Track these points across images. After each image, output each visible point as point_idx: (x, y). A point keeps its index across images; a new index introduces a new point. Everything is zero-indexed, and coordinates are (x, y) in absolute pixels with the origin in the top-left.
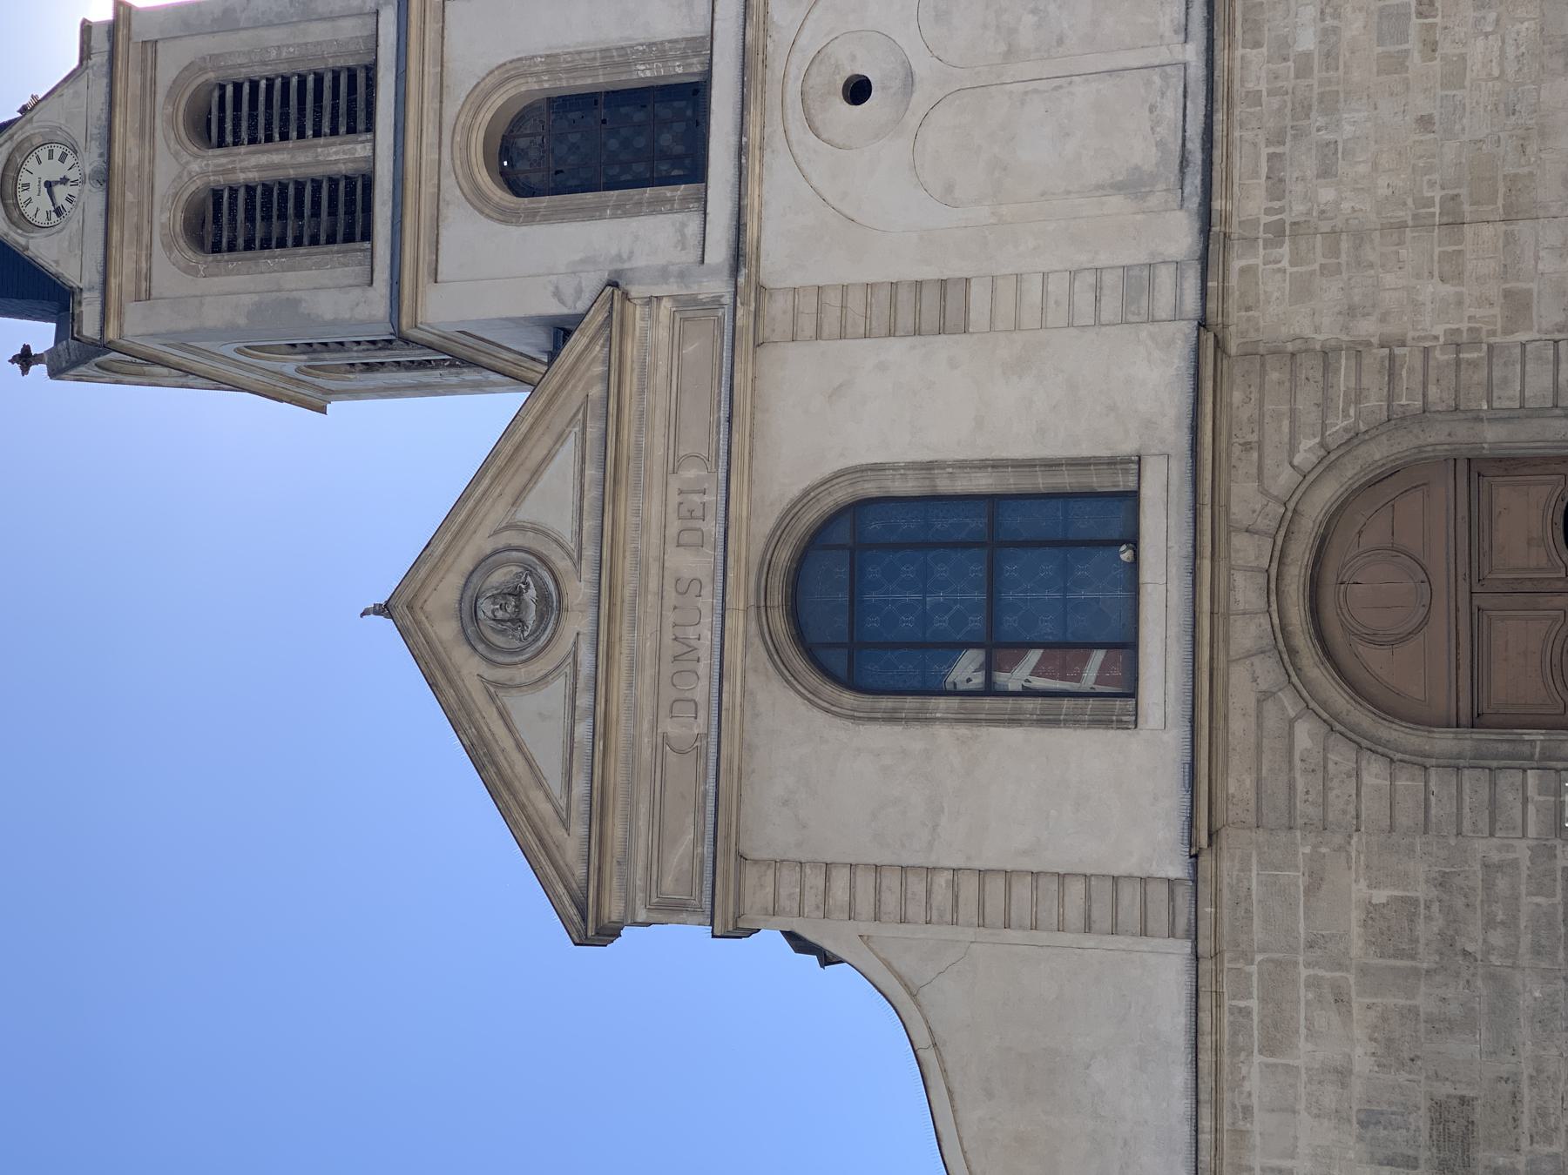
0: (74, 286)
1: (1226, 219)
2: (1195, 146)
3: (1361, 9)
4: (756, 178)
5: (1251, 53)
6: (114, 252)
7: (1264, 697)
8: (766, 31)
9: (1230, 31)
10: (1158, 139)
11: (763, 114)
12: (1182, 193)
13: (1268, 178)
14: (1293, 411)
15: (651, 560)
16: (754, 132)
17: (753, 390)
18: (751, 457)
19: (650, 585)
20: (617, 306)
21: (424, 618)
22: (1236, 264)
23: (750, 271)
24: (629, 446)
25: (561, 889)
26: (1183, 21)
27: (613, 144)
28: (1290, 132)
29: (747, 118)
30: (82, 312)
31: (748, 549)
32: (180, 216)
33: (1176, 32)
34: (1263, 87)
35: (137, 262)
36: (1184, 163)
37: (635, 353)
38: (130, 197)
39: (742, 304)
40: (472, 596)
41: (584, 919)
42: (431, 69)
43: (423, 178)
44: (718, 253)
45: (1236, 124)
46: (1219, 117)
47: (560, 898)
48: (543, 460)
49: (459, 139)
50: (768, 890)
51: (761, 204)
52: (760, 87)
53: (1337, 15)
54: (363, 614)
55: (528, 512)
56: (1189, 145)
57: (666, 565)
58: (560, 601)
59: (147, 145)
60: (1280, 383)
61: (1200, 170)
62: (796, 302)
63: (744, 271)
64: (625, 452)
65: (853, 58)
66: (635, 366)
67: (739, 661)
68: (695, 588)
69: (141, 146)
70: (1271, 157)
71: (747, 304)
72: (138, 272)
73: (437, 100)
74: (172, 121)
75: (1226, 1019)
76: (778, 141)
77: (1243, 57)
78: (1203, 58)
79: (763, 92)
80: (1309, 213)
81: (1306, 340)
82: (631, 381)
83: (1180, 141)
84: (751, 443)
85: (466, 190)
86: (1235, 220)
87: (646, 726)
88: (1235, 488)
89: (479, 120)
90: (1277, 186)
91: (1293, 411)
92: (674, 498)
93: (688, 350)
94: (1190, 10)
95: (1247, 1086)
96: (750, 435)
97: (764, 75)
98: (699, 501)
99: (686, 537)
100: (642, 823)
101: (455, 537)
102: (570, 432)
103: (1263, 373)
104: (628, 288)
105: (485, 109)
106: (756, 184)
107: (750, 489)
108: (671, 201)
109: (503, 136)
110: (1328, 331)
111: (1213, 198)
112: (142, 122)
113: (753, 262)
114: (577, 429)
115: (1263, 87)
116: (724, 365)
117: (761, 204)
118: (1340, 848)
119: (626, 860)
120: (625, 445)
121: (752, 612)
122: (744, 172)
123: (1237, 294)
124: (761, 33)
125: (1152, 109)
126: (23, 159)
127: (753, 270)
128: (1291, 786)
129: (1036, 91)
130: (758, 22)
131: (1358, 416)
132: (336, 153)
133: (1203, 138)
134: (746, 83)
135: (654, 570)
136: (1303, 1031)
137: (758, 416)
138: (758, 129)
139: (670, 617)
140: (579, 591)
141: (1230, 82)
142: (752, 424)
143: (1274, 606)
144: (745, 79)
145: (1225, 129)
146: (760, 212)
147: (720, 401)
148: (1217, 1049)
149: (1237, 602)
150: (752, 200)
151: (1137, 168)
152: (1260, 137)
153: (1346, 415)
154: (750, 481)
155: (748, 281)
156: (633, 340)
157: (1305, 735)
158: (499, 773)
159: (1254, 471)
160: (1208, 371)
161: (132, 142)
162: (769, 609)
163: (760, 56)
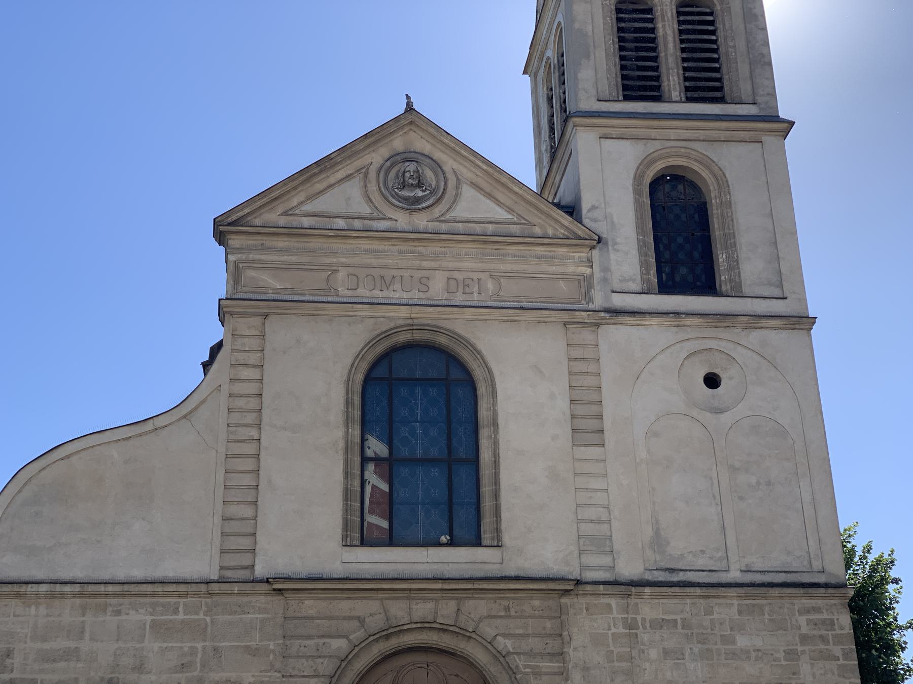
1: (639, 595)
2: (681, 577)
3: (761, 672)
5: (735, 609)
7: (361, 621)
8: (746, 328)
9: (747, 597)
10: (685, 556)
11: (698, 326)
12: (654, 570)
13: (663, 620)
14: (528, 635)
15: (440, 262)
16: (688, 321)
17: (539, 322)
18: (500, 321)
19: (425, 262)
20: (587, 242)
22: (613, 602)
25: (246, 211)
26: (753, 569)
27: (680, 240)
28: (689, 632)
29: (696, 317)
31: (446, 319)
33: (747, 565)
34: (715, 616)
36: (672, 570)
37: (560, 253)
39: (589, 315)
40: (418, 159)
41: (229, 224)
44: (619, 301)
45: (694, 601)
46: (698, 591)
47: (242, 210)
50: (247, 331)
52: (713, 324)
53: (757, 659)
54: (407, 95)
55: (467, 192)
56: (681, 573)
60: (544, 628)
61: (667, 580)
63: (607, 316)
64: (502, 247)
65: (731, 378)
67: (381, 314)
68: (424, 288)
70: (675, 621)
75: (173, 600)
76: (682, 336)
77: (733, 604)
78: (732, 581)
80: (643, 644)
81: (569, 643)
83: (684, 568)
84: (507, 321)
85: (653, 155)
86: (638, 601)
87: (343, 260)
88: (483, 602)
90: (658, 624)
91: (528, 635)
93: (562, 284)
94: (760, 574)
95: (132, 612)
97: (720, 327)
98: (474, 291)
100: (286, 258)
103: (550, 618)
104: (598, 249)
107: (480, 320)
109: (684, 177)
110: (574, 655)
111: (651, 588)
113: (613, 321)
114: (515, 219)
115: (715, 616)
117: (646, 325)
118: (272, 666)
119: (265, 249)
120: (507, 248)
121: (410, 322)
122: (665, 316)
123: (596, 602)
124: (745, 325)
125: (703, 552)
127: (608, 321)
128: (309, 637)
129: (712, 484)
130: (751, 323)
131: (526, 674)
132: (674, 80)
133: (685, 581)
134: (715, 316)
136: (165, 645)
139: (406, 274)
140: (421, 221)
141: (718, 597)
143: (414, 626)
145: (690, 594)
146: (642, 325)
147: (532, 302)
148: (154, 595)
149: (417, 604)
150: (649, 321)
151: (668, 543)
152: (687, 614)
153: (526, 667)
154: (486, 320)
156: (567, 252)
157: (339, 645)
158: (315, 175)
159: (493, 613)
160: (551, 586)
162: (412, 331)
163: (731, 325)
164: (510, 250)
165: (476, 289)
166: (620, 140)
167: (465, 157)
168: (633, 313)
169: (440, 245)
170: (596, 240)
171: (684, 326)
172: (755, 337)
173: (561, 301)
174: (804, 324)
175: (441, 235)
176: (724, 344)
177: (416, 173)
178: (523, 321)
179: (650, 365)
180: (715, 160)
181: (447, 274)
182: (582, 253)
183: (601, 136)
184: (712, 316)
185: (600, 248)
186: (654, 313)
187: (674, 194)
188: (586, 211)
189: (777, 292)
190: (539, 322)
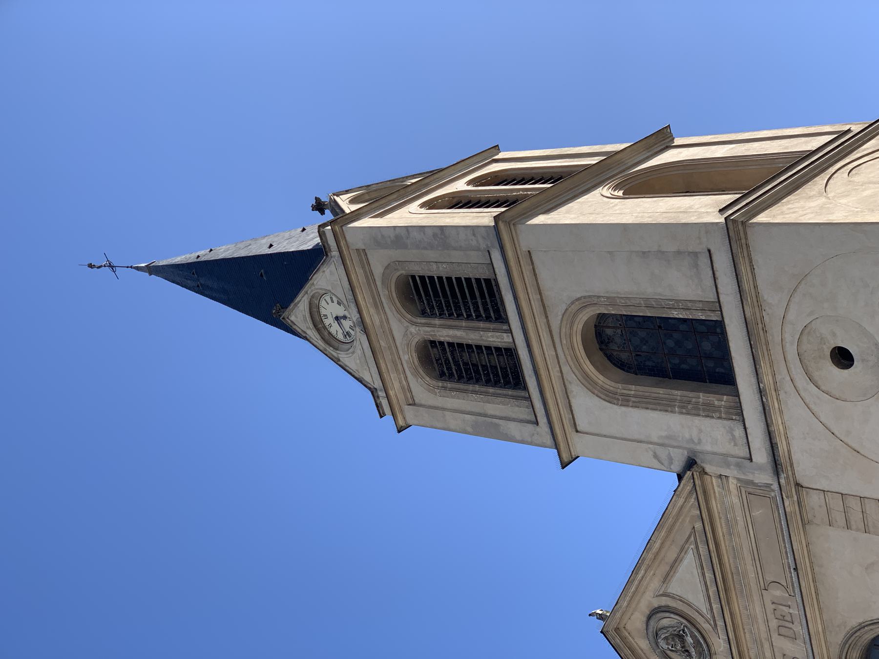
0: (372, 387)
4: (777, 410)
6: (385, 375)
8: (760, 307)
11: (772, 366)
16: (767, 380)
17: (809, 552)
18: (817, 594)
19: (766, 654)
20: (698, 482)
21: (627, 634)
23: (788, 475)
24: (730, 566)
27: (670, 343)
29: (760, 371)
30: (380, 401)
31: (828, 649)
32: (415, 355)
35: (400, 382)
38: (383, 344)
39: (787, 497)
40: (653, 632)
42: (534, 297)
43: (550, 368)
44: (761, 456)
48: (675, 561)
49: (565, 342)
51: (785, 428)
52: (764, 347)
54: (590, 615)
55: (674, 588)
57: (774, 644)
58: (709, 650)
59: (381, 311)
62: (827, 501)
63: (783, 476)
65: (834, 335)
66: (721, 515)
69: (378, 313)
71: (791, 497)
72: (403, 388)
73: (544, 317)
74: (390, 298)
76: (788, 386)
79: (768, 350)
82: (721, 525)
89: (575, 328)
92: (770, 607)
93: (756, 513)
96: (813, 581)
98: (787, 612)
99: (783, 631)
101: (631, 599)
102: (688, 547)
105: (576, 323)
106: (778, 414)
107: (821, 614)
108: (717, 409)
109: (595, 325)
112: (374, 298)
113: (789, 468)
116: (784, 529)
117: (785, 428)
120: (727, 565)
124: (757, 309)
126: (318, 300)
127: (790, 473)
132: (492, 337)
134: (753, 346)
135: (766, 645)
137: (816, 569)
138: (770, 378)
142: (813, 573)
144: (752, 343)
150: (786, 356)
154: (820, 609)
155: (788, 483)
161: (372, 311)
163: (760, 326)
164: (729, 561)
165: (785, 609)
166: (573, 409)
167: (637, 589)
168: (773, 447)
169: (742, 635)
170: (693, 474)
171: (775, 383)
172: (773, 300)
173: (777, 518)
174: (738, 233)
175: (731, 637)
176: (787, 337)
177: (669, 641)
178: (812, 569)
179: (836, 433)
180: (564, 307)
181: (775, 636)
182: (712, 483)
183: (574, 430)
184: (754, 350)
185: (701, 462)
186: (766, 421)
187: (618, 340)
188: (663, 466)
189: (704, 261)
190: (809, 552)
